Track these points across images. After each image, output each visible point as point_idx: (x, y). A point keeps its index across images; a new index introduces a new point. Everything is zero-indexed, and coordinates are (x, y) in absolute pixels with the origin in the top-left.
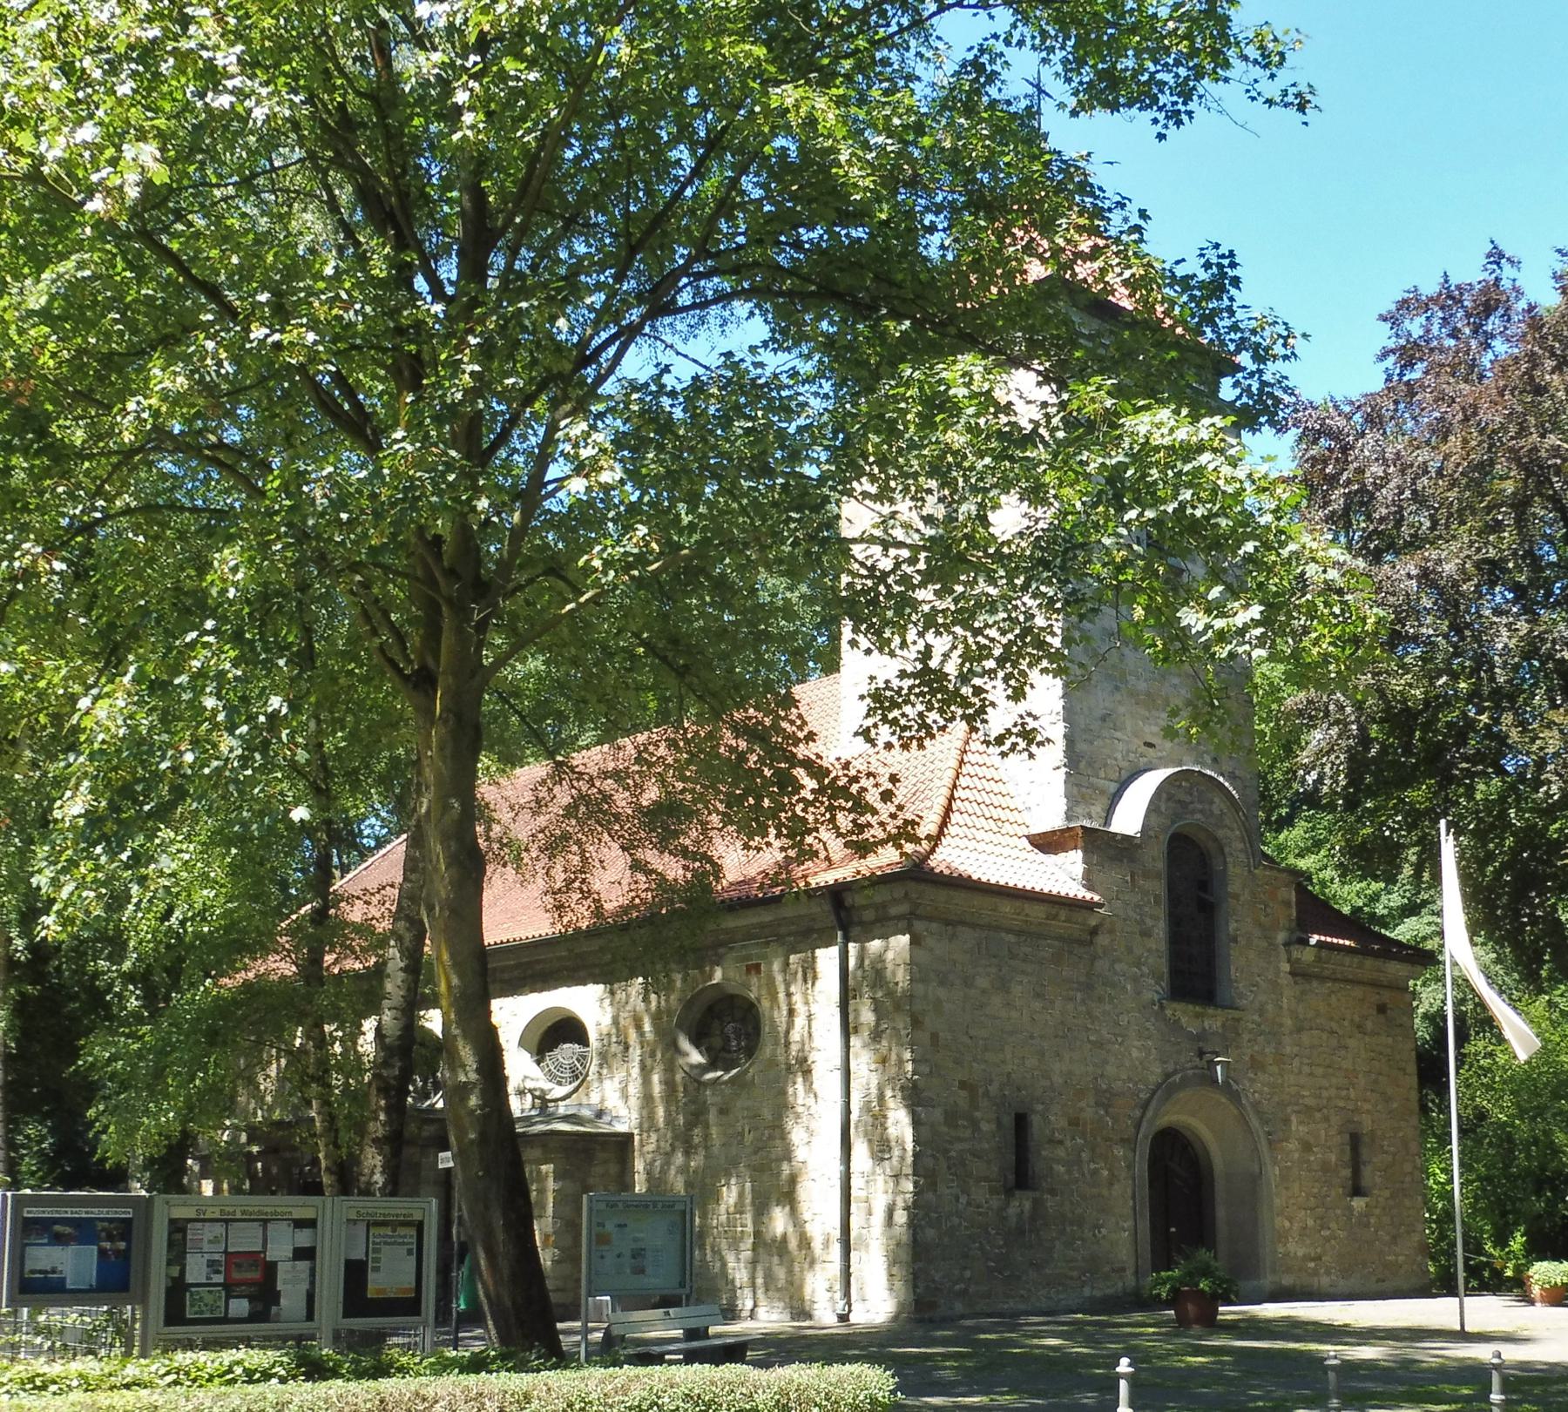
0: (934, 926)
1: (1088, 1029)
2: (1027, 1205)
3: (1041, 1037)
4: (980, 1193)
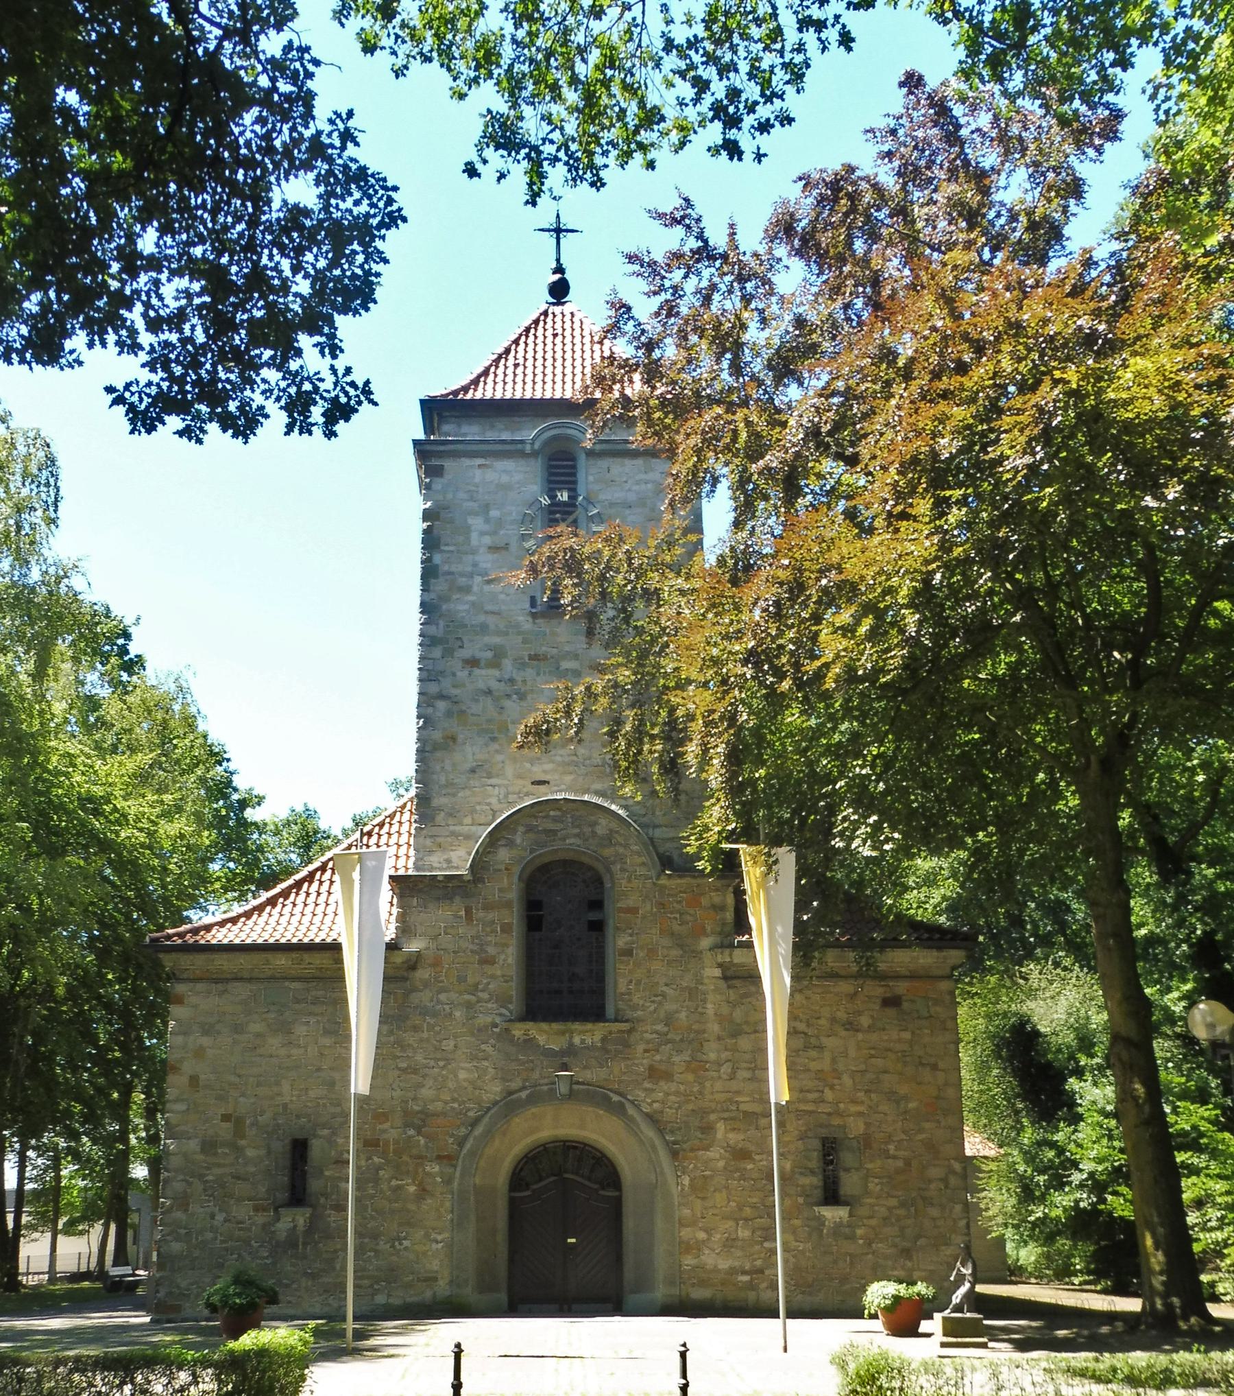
0: (200, 986)
1: (396, 1057)
2: (301, 1221)
3: (331, 1069)
4: (243, 1211)
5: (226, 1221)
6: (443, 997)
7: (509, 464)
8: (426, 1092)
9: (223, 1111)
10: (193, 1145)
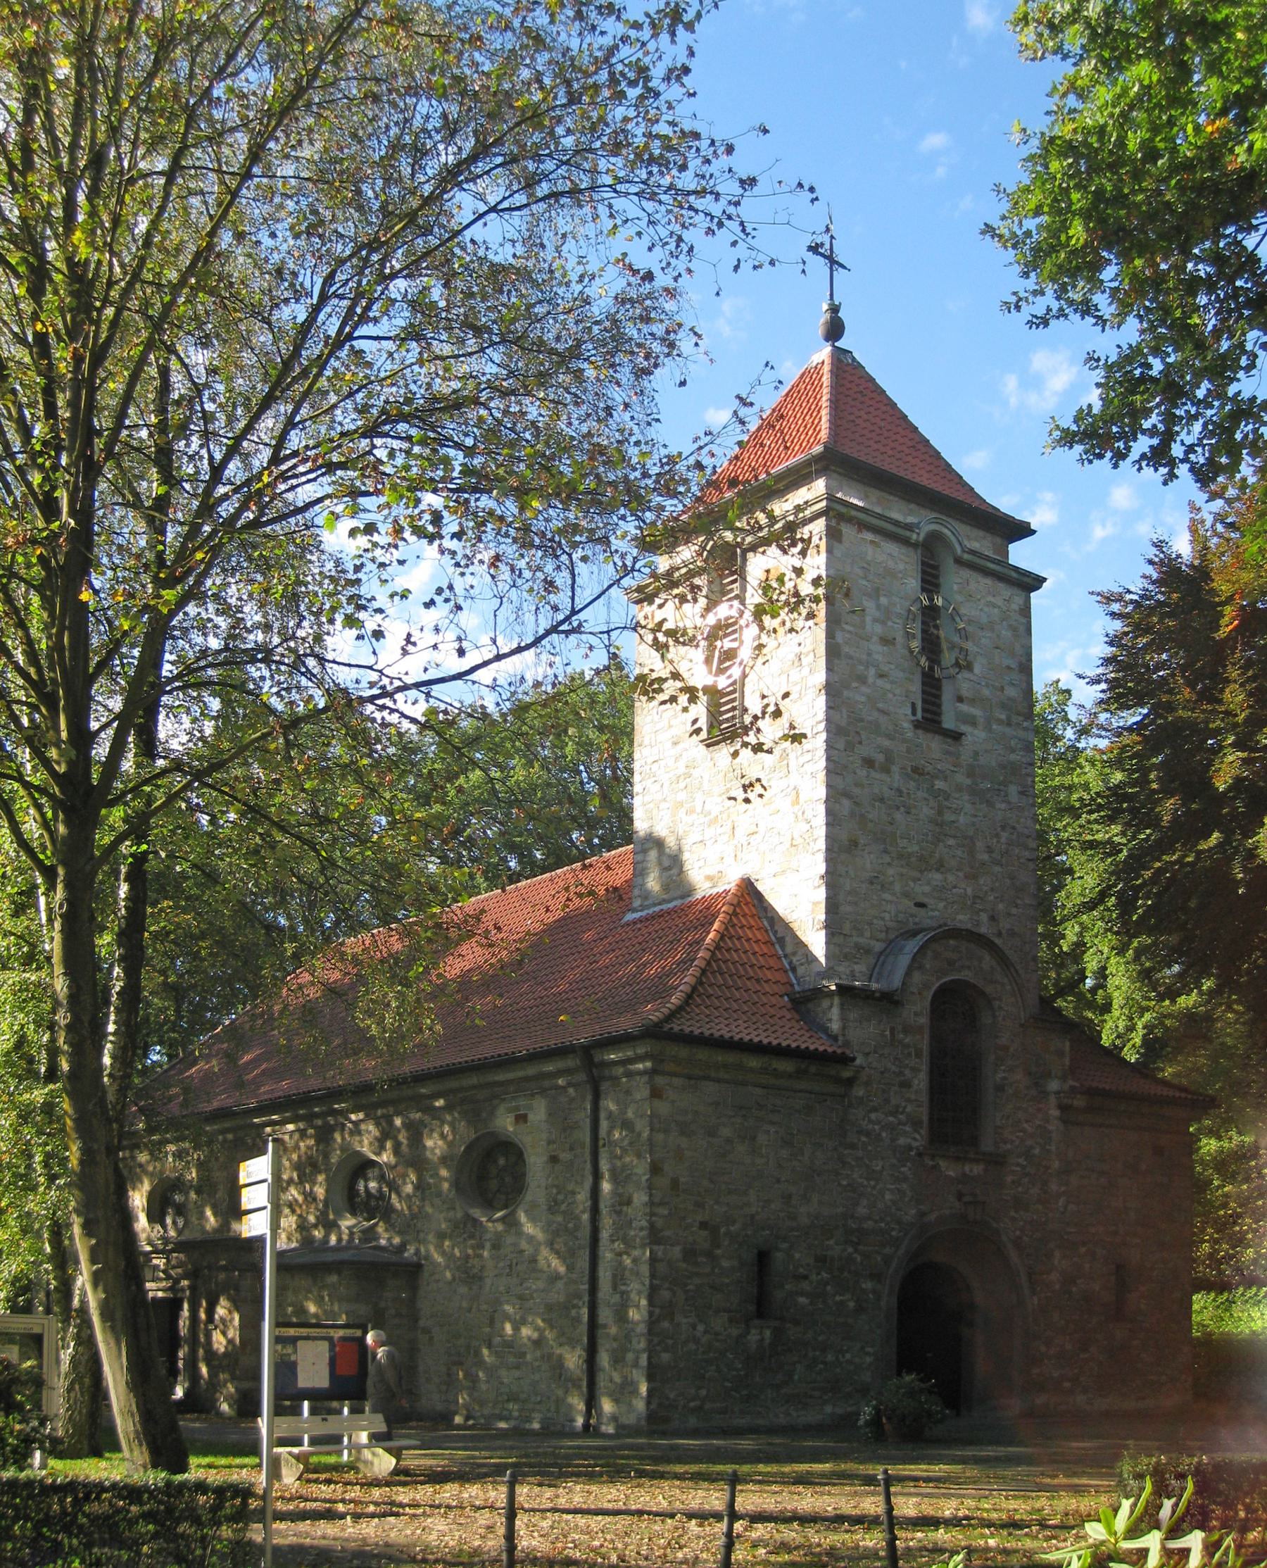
5: (706, 1332)
6: (873, 1116)
7: (891, 548)
8: (862, 1211)
9: (699, 1218)
10: (676, 1252)
